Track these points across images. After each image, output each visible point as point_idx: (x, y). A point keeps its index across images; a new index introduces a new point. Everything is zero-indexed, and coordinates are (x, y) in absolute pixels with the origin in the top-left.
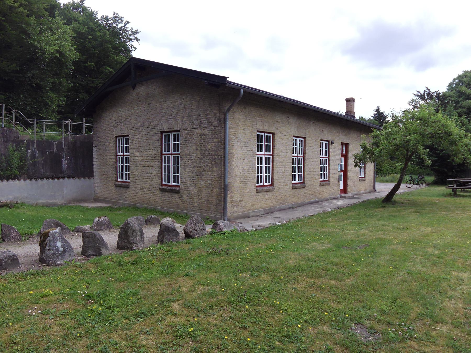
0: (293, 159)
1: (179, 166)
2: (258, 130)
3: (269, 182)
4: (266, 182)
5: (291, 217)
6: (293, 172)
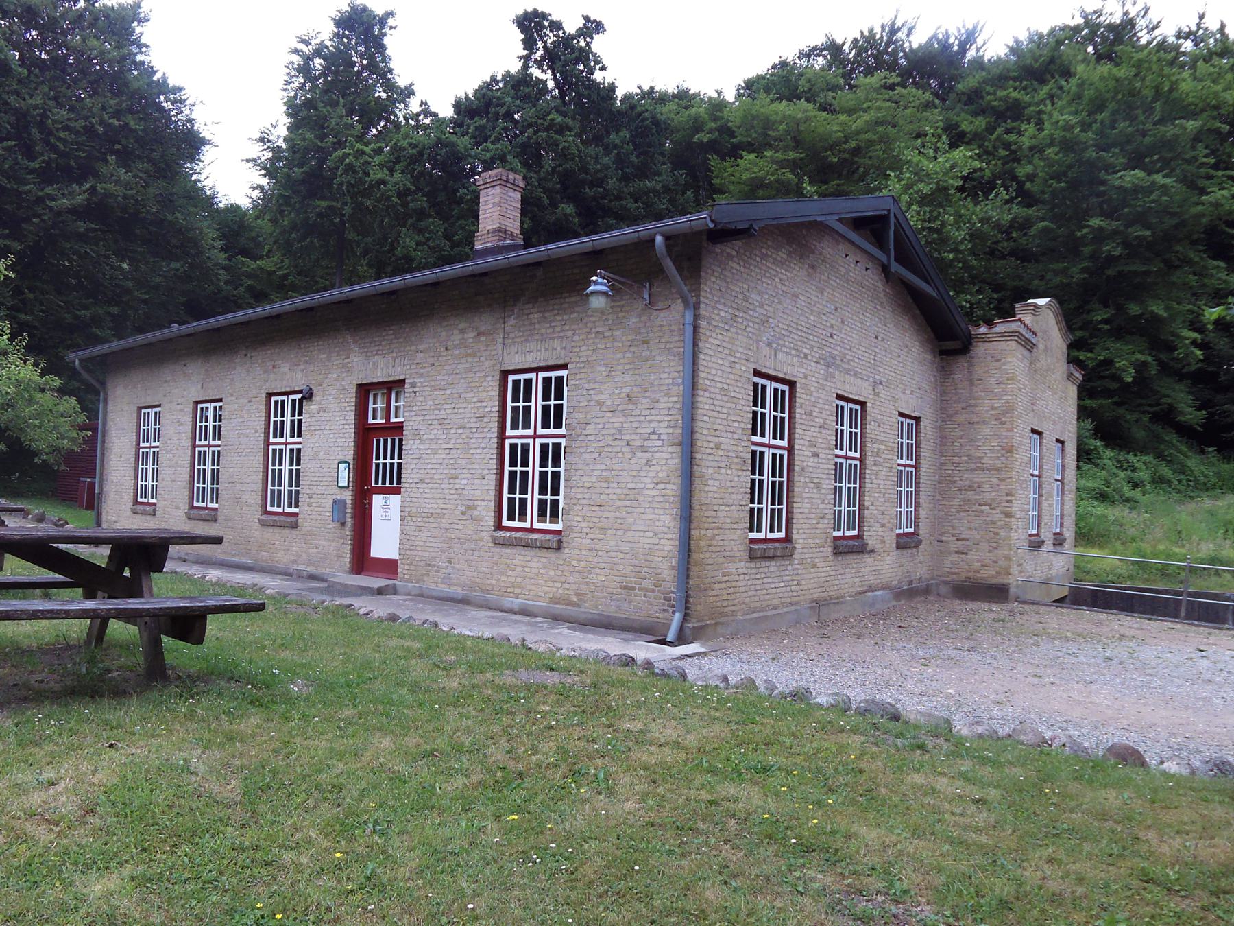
0: (754, 453)
1: (559, 472)
2: (759, 369)
3: (780, 530)
4: (772, 531)
5: (584, 645)
6: (752, 502)
